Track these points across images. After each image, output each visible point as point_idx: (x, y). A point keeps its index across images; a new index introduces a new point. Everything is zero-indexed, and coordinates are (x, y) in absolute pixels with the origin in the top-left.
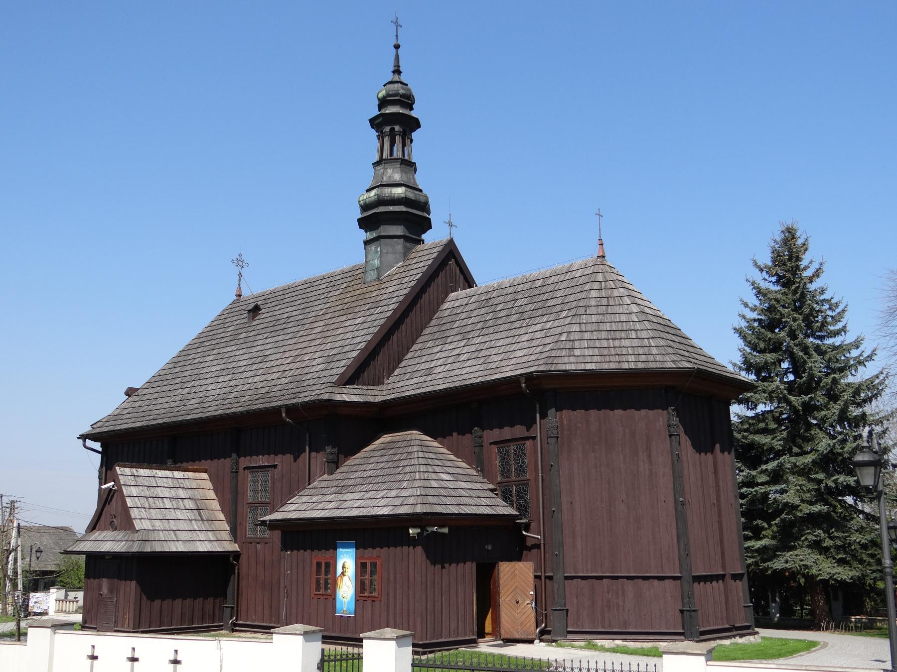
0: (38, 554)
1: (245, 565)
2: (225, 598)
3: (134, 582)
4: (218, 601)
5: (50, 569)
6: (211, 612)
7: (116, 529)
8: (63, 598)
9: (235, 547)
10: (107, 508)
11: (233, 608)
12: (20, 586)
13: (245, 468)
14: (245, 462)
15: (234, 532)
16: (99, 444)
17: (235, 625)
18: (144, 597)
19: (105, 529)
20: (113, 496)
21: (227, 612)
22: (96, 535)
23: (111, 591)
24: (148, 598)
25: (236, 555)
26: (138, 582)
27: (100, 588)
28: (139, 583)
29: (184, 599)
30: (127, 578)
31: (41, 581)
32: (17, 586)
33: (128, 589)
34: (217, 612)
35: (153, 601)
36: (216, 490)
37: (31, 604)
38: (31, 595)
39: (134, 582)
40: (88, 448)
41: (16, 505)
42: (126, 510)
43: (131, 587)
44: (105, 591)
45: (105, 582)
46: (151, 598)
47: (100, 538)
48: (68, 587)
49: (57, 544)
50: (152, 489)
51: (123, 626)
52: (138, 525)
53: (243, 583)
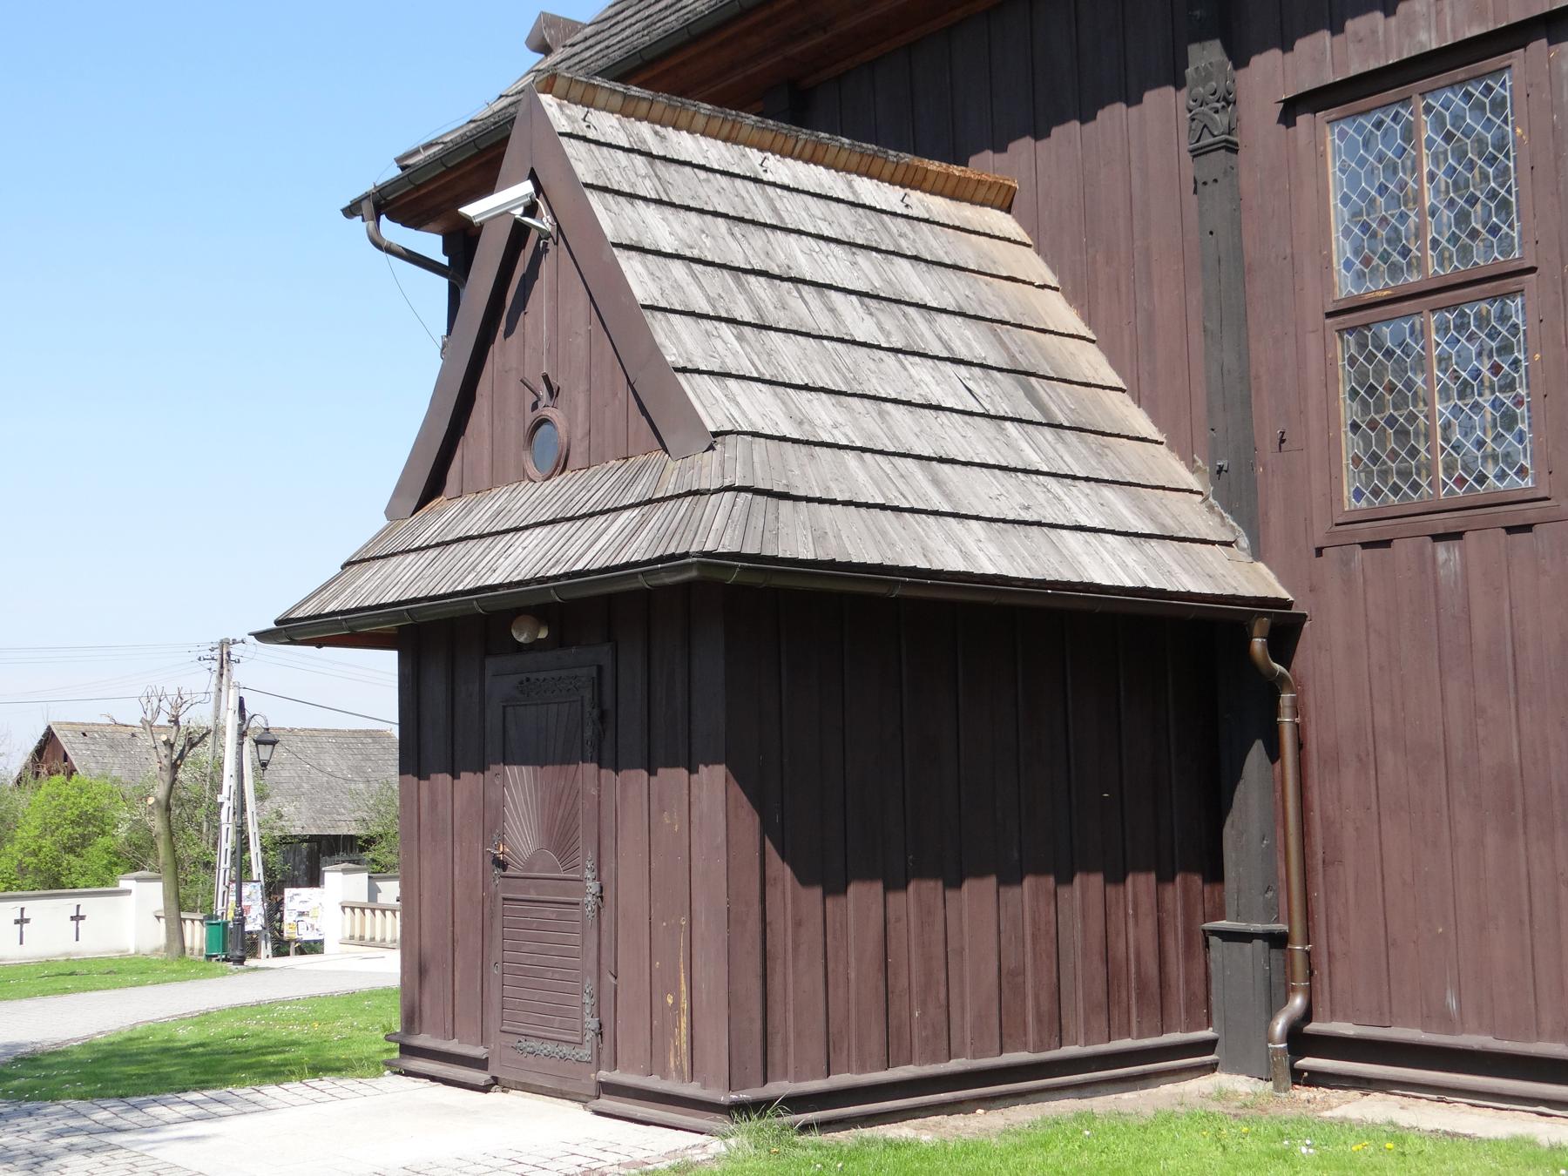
0: (265, 752)
1: (1328, 685)
2: (1214, 872)
3: (713, 780)
4: (1173, 894)
5: (343, 830)
6: (1152, 969)
7: (562, 465)
8: (363, 898)
9: (1250, 578)
10: (502, 353)
11: (1278, 941)
12: (257, 870)
13: (1292, 109)
14: (1273, 74)
15: (1235, 488)
16: (437, 240)
17: (1300, 1041)
18: (782, 872)
19: (497, 480)
20: (538, 254)
21: (1236, 969)
22: (446, 516)
23: (560, 838)
24: (805, 878)
25: (1285, 627)
26: (739, 773)
27: (491, 820)
28: (755, 782)
29: (1009, 878)
30: (664, 747)
31: (307, 858)
32: (249, 870)
33: (671, 821)
34: (1176, 969)
35: (834, 888)
36: (1078, 292)
37: (289, 918)
38: (288, 892)
39: (713, 780)
40: (389, 250)
41: (236, 651)
42: (618, 322)
43: (696, 812)
44: (523, 837)
45: (519, 789)
46: (826, 871)
47: (474, 524)
48: (378, 872)
49: (358, 770)
50: (758, 237)
51: (654, 1065)
52: (713, 404)
53: (1340, 797)
